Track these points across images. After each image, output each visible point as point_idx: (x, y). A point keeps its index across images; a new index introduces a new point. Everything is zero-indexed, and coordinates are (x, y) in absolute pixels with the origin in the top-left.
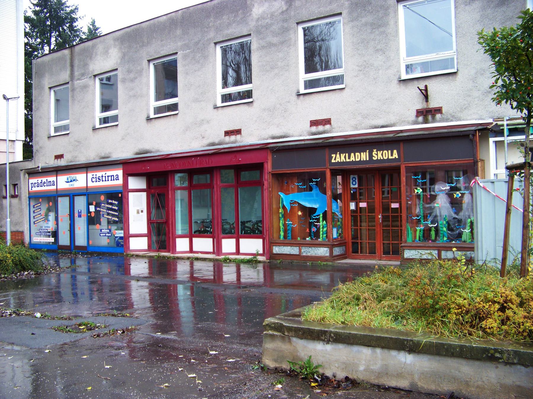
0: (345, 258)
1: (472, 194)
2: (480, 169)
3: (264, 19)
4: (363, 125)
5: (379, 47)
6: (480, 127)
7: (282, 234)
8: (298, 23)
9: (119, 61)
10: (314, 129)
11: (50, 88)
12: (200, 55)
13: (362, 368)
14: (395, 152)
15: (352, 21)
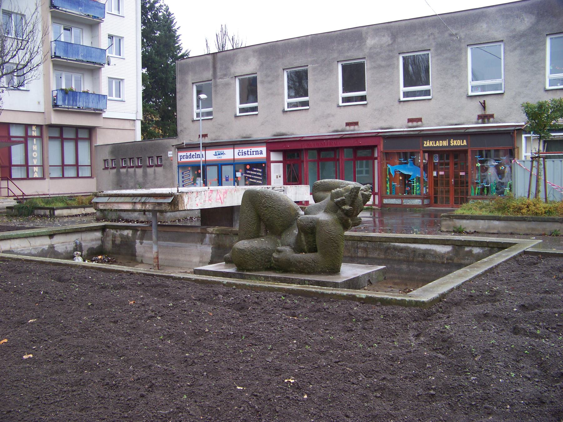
0: (430, 206)
1: (511, 168)
2: (516, 153)
3: (375, 48)
4: (443, 123)
5: (454, 74)
6: (517, 128)
7: (388, 191)
8: (399, 54)
9: (258, 68)
10: (410, 124)
11: (193, 83)
12: (326, 69)
13: (480, 228)
14: (465, 141)
15: (437, 55)
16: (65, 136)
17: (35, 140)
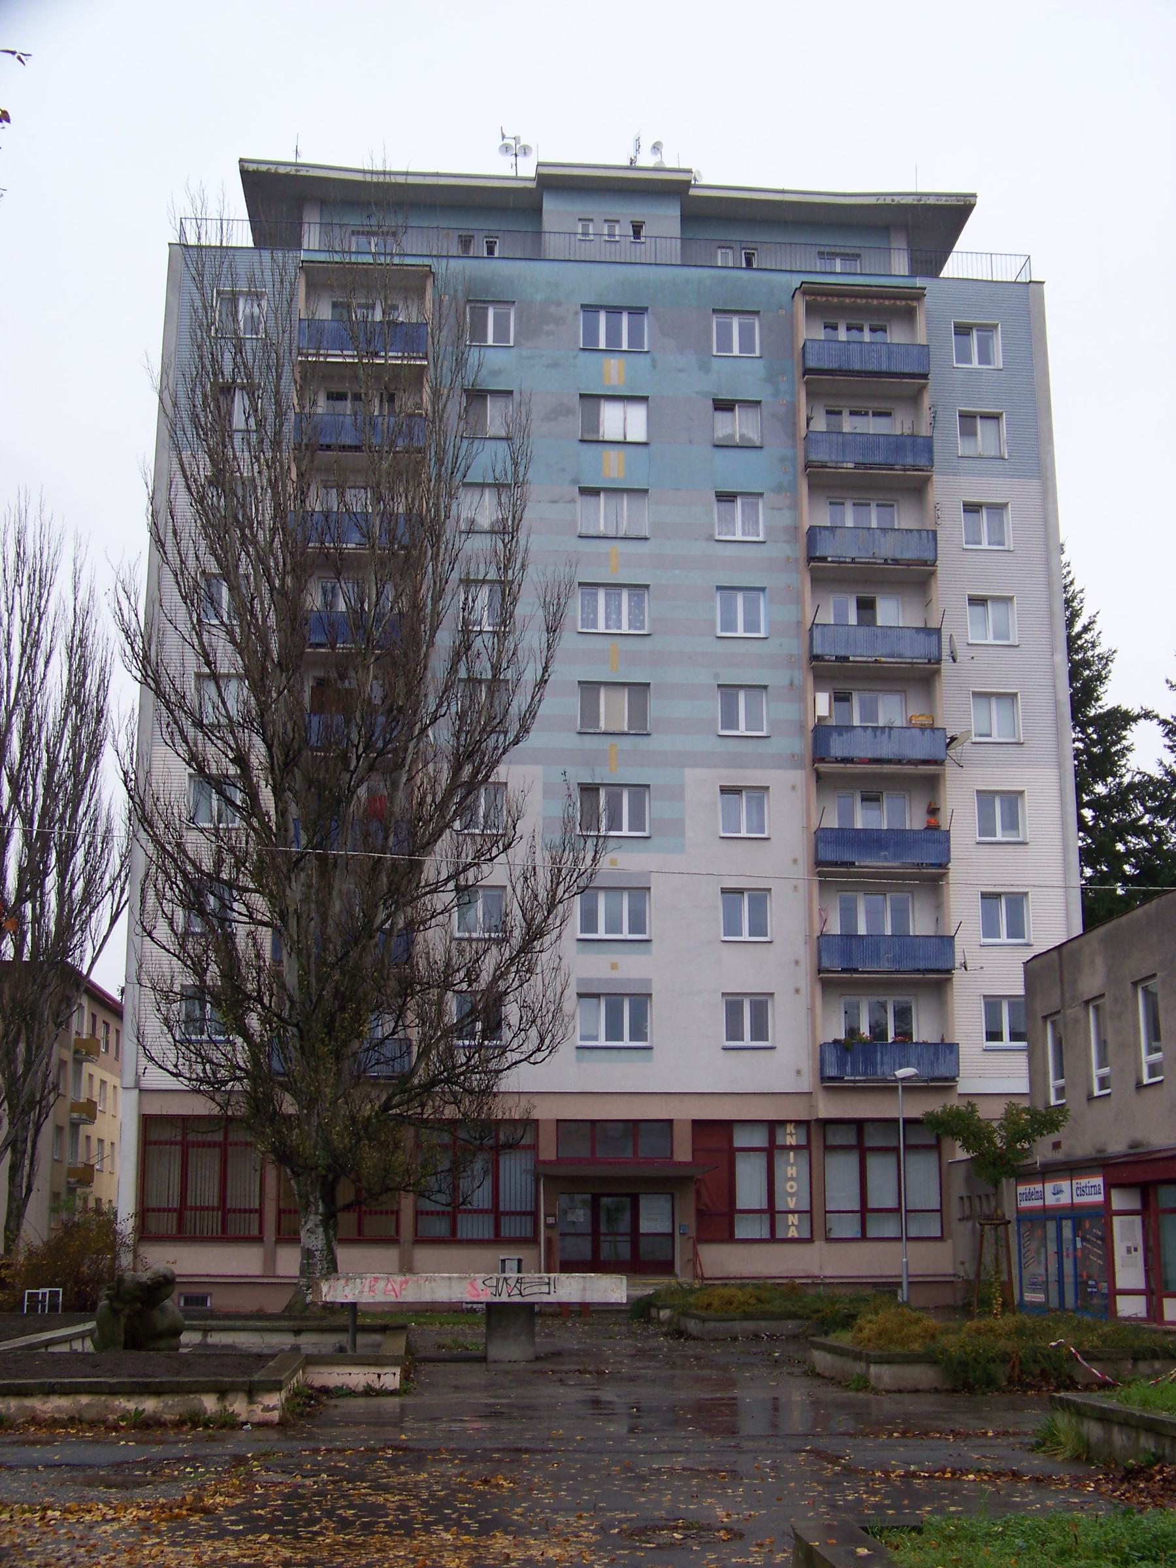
17: (792, 1154)
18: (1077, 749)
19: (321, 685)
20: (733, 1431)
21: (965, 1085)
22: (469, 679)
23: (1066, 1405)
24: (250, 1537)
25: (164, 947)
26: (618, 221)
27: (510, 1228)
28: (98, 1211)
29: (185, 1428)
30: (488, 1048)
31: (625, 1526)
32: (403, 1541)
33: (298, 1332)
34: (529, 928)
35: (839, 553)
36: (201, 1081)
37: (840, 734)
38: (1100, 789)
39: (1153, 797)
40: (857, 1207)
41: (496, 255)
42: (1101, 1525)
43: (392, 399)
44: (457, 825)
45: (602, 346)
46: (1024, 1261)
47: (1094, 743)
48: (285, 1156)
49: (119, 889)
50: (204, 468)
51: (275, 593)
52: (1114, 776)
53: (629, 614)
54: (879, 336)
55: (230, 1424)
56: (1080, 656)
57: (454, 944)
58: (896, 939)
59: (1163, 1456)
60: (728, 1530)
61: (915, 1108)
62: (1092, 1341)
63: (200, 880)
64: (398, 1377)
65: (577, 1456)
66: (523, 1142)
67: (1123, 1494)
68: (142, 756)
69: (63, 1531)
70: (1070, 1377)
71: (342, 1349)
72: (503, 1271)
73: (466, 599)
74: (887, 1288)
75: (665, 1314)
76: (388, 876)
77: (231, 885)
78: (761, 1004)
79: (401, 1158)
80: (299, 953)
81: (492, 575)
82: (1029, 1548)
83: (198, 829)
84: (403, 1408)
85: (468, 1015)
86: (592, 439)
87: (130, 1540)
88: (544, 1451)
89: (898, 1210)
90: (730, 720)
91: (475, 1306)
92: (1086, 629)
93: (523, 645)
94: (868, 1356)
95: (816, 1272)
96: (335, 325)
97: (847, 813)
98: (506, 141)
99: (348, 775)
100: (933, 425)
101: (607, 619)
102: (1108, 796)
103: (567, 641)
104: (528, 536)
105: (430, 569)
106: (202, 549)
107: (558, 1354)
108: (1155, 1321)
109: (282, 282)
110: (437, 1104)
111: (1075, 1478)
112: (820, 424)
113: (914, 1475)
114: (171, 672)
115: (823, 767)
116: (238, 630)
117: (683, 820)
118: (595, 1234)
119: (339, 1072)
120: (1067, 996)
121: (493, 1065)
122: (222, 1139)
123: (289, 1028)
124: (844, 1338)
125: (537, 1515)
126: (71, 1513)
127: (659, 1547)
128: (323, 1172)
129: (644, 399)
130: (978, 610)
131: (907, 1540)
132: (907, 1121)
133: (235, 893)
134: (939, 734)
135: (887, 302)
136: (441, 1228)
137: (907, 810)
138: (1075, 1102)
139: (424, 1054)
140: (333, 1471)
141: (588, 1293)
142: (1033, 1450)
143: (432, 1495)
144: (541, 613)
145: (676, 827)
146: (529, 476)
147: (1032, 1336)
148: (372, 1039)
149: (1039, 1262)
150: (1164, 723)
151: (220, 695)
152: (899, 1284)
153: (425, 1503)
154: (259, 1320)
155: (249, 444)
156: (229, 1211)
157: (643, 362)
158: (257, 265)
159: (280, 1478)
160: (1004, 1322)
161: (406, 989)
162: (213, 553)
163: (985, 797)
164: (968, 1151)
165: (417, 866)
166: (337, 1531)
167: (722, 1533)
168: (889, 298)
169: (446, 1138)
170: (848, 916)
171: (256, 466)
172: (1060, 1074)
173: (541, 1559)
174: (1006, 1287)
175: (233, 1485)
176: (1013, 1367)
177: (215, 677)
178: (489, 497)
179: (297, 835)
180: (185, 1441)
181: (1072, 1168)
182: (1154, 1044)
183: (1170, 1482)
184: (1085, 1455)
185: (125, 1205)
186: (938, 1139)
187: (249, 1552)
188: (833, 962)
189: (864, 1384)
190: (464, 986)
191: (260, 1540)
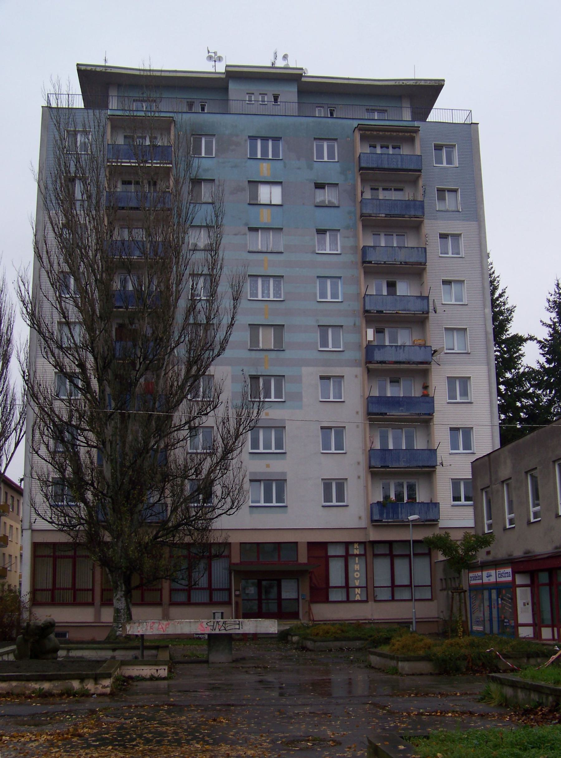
16: (395, 553)
17: (357, 558)
18: (496, 356)
19: (121, 327)
20: (329, 695)
21: (443, 523)
22: (195, 324)
23: (494, 679)
24: (102, 748)
25: (44, 459)
26: (266, 94)
27: (217, 597)
28: (10, 591)
29: (64, 697)
30: (206, 507)
31: (284, 740)
32: (177, 749)
33: (114, 650)
34: (226, 448)
35: (378, 259)
36: (64, 525)
37: (379, 350)
38: (508, 375)
39: (534, 379)
40: (389, 584)
41: (206, 111)
42: (514, 733)
43: (155, 184)
44: (189, 397)
45: (259, 157)
46: (472, 610)
47: (505, 353)
48: (105, 562)
49: (19, 429)
50: (61, 220)
51: (98, 282)
52: (515, 369)
53: (274, 290)
54: (397, 151)
55: (86, 694)
56: (498, 309)
57: (189, 456)
58: (407, 451)
59: (542, 703)
60: (334, 741)
61: (420, 535)
62: (507, 649)
63: (62, 425)
64: (166, 671)
65: (258, 707)
66: (223, 554)
67: (523, 721)
68: (31, 363)
69: (11, 746)
70: (497, 667)
71: (136, 658)
72: (214, 618)
73: (193, 284)
74: (406, 624)
75: (295, 639)
76: (156, 422)
77: (77, 427)
78: (341, 484)
79: (163, 563)
80: (112, 461)
81: (206, 271)
82: (480, 744)
83: (60, 399)
84: (169, 685)
85: (196, 491)
86: (254, 203)
87: (45, 750)
88: (242, 705)
89: (410, 586)
90: (324, 343)
91: (200, 636)
92: (501, 296)
93: (222, 306)
94: (398, 658)
95: (370, 617)
96: (126, 147)
97: (383, 389)
98: (210, 54)
99: (135, 372)
100: (424, 195)
101: (263, 293)
102: (512, 378)
103: (243, 304)
104: (224, 251)
105: (175, 269)
106: (62, 260)
107: (244, 659)
108: (537, 639)
109: (99, 126)
110: (181, 535)
111: (501, 715)
112: (368, 195)
113: (422, 714)
114: (47, 322)
115: (371, 366)
116: (80, 300)
117: (301, 393)
118: (260, 600)
119: (132, 520)
120: (493, 479)
121: (209, 516)
122: (73, 554)
123: (107, 499)
124: (385, 649)
125: (240, 735)
126: (14, 738)
127: (301, 749)
128: (125, 570)
129: (280, 183)
130: (447, 287)
131: (422, 742)
132: (415, 542)
133: (79, 431)
134: (428, 349)
135: (400, 134)
136: (182, 597)
137: (413, 384)
138: (497, 531)
139: (174, 510)
140: (139, 716)
141: (258, 628)
142: (479, 702)
143: (189, 727)
144: (230, 290)
145: (297, 397)
146: (224, 221)
147: (478, 646)
148: (149, 503)
149: (480, 611)
150: (540, 342)
151: (71, 333)
152: (411, 623)
153: (186, 730)
154: (92, 644)
155: (83, 207)
156: (77, 590)
157: (279, 165)
158: (86, 117)
159: (113, 720)
160: (464, 640)
161: (165, 478)
162: (67, 262)
163: (451, 380)
164: (445, 556)
165: (170, 418)
166: (145, 744)
167: (331, 743)
168: (402, 132)
169: (185, 552)
170: (384, 440)
171: (87, 218)
172: (490, 518)
173: (244, 755)
174: (465, 623)
175: (91, 723)
176: (469, 662)
177: (68, 324)
178: (203, 233)
179: (110, 403)
180: (65, 703)
181: (496, 564)
182: (536, 502)
183: (546, 715)
184: (505, 703)
185: (26, 589)
186: (430, 549)
187: (103, 755)
188: (376, 463)
189: (395, 671)
190: (194, 477)
191: (108, 749)
